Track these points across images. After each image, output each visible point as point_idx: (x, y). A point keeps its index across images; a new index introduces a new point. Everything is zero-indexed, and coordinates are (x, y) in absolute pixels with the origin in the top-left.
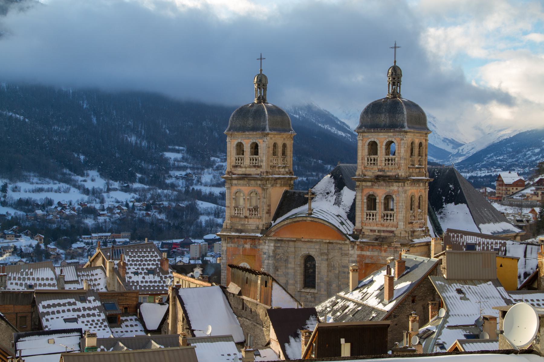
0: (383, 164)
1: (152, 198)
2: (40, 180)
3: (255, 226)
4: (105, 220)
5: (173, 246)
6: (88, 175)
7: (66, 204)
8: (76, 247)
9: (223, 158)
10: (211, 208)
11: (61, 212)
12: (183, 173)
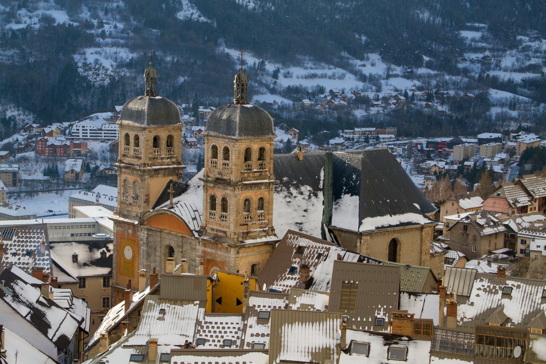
0: (221, 168)
1: (437, 86)
2: (315, 65)
3: (136, 213)
4: (378, 111)
5: (439, 146)
6: (368, 59)
7: (339, 93)
8: (333, 143)
9: (533, 36)
10: (506, 99)
11: (330, 101)
12: (481, 56)
